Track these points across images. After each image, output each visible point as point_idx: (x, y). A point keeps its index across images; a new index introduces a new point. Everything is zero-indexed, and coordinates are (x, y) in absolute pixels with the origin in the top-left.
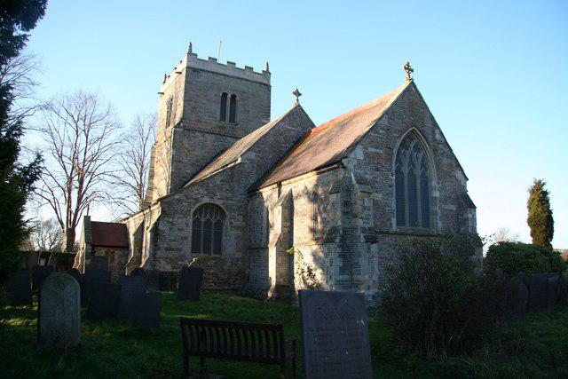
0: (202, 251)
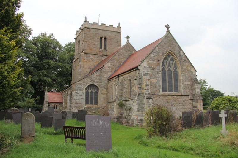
0: (90, 104)
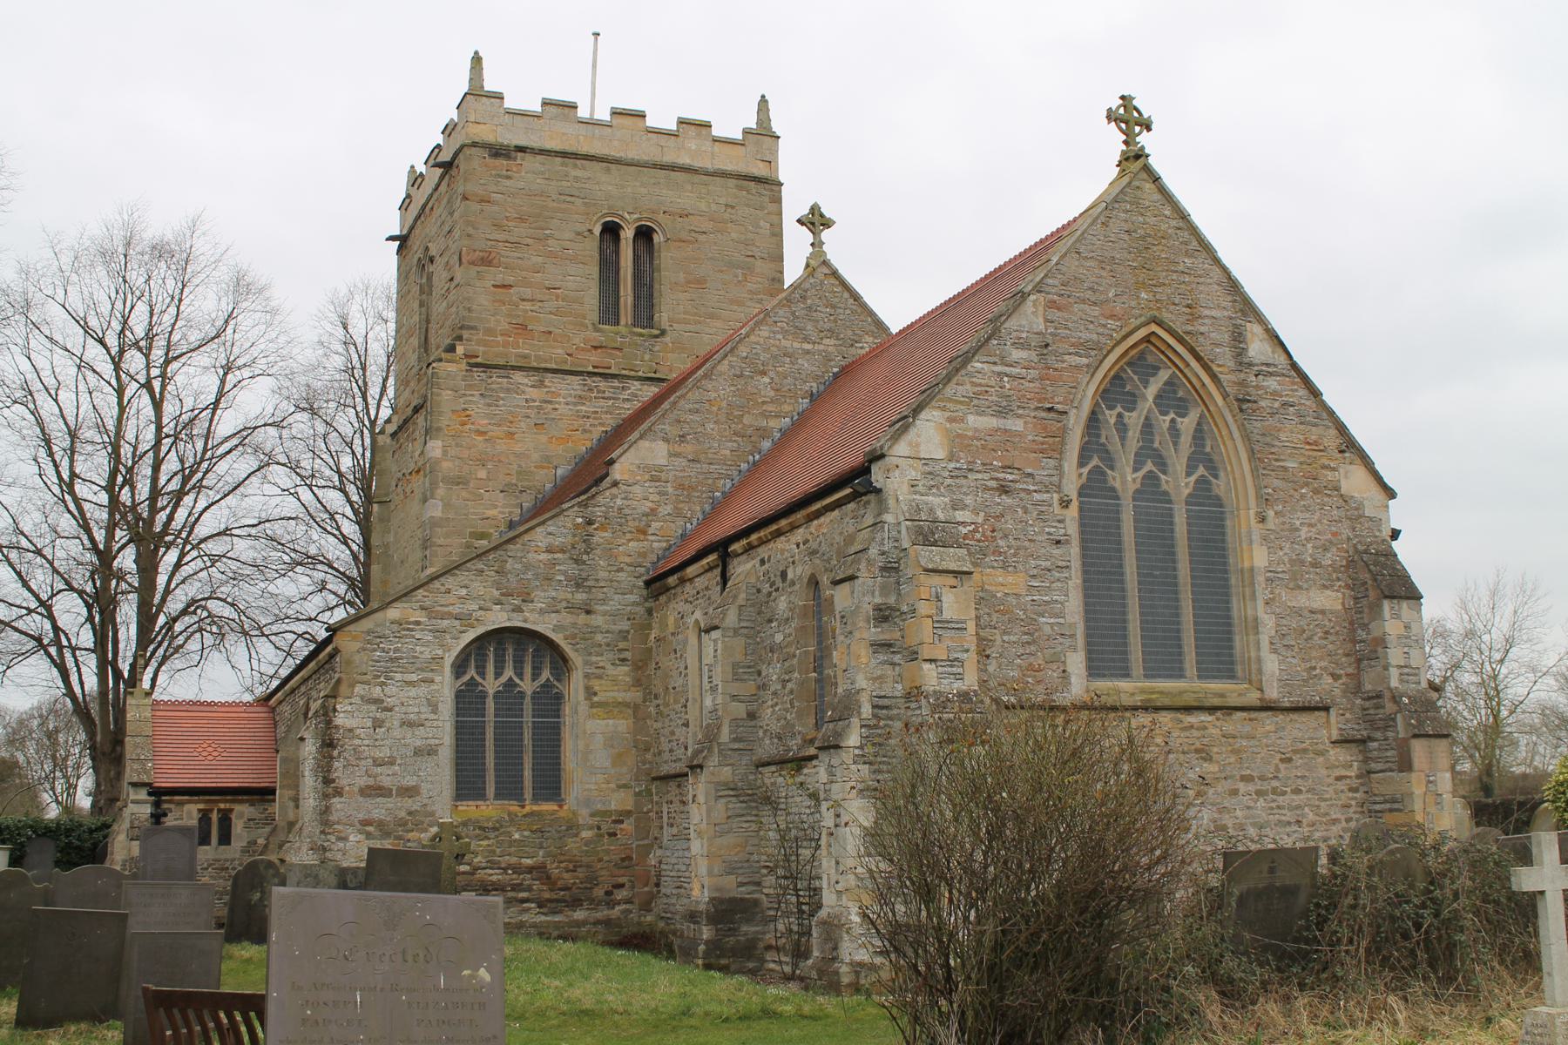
0: (491, 790)
